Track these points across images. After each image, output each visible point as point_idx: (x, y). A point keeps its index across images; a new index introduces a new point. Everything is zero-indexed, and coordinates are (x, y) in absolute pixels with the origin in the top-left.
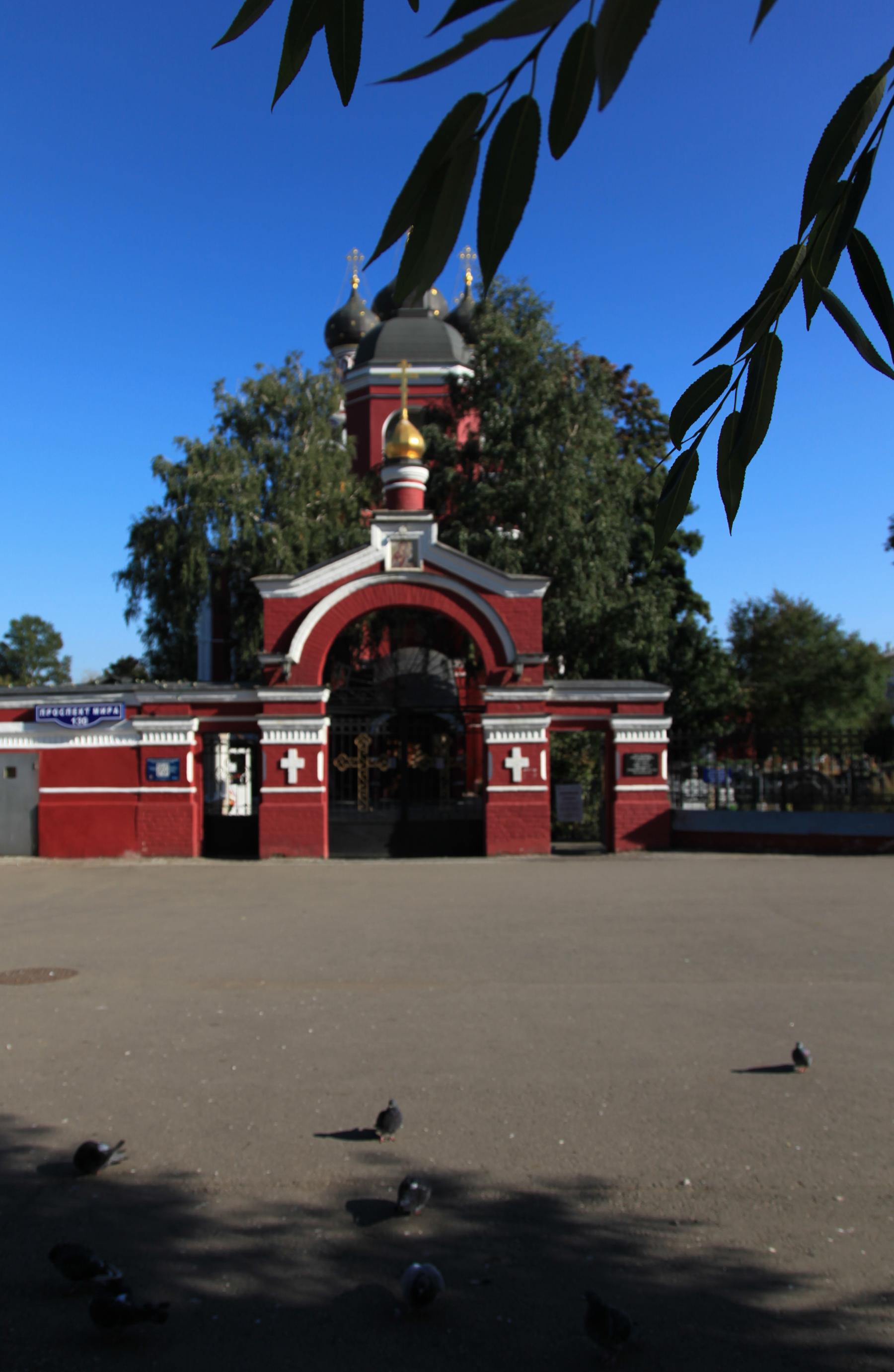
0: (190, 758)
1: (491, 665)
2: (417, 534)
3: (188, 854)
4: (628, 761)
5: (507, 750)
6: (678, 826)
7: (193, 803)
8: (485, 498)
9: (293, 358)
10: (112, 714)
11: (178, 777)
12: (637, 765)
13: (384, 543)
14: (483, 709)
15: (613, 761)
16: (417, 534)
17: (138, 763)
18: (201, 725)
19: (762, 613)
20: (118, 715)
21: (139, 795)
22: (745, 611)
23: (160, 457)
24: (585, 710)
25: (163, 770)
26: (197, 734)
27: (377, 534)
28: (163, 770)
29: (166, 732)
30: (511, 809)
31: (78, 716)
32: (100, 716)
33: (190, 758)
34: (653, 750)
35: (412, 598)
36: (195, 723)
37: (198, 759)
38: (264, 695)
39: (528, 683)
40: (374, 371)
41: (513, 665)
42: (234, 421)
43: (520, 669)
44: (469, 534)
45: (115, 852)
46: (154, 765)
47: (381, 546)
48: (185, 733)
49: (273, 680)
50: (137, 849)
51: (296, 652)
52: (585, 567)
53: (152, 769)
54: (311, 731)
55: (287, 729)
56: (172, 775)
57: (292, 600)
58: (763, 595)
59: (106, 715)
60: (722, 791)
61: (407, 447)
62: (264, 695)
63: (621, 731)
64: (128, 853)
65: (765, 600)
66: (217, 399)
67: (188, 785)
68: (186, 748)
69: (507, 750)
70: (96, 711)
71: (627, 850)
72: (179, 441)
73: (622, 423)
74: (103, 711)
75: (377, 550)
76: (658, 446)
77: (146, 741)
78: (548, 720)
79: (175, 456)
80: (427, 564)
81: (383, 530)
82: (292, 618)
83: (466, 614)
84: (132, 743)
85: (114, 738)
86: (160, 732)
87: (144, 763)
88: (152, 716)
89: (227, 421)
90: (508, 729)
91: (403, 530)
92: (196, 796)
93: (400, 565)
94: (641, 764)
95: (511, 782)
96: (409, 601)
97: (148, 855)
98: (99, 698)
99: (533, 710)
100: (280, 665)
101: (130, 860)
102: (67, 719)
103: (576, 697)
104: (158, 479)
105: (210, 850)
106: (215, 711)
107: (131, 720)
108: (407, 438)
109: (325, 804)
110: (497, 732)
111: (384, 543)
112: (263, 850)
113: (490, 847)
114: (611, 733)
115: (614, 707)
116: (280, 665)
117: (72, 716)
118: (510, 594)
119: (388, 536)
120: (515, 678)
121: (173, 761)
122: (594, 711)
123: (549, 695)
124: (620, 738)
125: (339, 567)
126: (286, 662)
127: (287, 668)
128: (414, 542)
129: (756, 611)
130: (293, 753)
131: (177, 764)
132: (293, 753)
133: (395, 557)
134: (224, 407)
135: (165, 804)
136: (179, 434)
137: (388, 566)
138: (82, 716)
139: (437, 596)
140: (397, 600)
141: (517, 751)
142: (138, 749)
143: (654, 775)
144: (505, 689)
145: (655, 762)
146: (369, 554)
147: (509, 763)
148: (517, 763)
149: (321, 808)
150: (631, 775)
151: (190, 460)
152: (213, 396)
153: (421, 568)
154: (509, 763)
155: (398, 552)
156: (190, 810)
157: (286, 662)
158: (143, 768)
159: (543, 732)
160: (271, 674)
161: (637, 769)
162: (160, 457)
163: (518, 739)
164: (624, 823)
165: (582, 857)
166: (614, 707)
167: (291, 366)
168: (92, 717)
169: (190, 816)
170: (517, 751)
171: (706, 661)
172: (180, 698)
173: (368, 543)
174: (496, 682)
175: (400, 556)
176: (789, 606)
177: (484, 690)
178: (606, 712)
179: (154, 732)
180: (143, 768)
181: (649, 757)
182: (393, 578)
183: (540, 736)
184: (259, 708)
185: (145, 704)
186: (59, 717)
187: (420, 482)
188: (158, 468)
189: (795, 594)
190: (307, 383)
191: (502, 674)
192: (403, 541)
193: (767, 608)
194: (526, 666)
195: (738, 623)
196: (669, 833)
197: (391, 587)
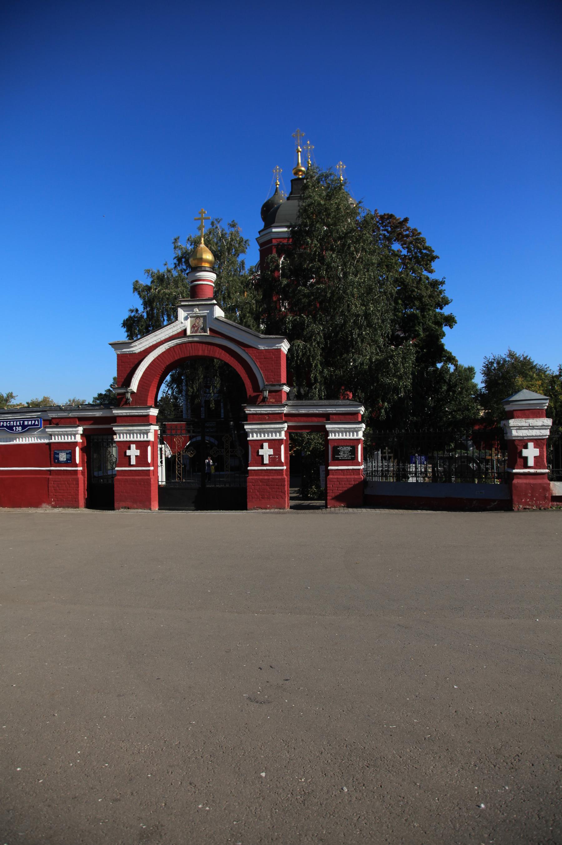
0: (77, 449)
1: (250, 392)
2: (205, 312)
3: (77, 507)
4: (336, 451)
5: (260, 444)
6: (368, 492)
7: (80, 476)
8: (305, 296)
9: (215, 222)
10: (34, 425)
11: (71, 461)
12: (341, 453)
13: (186, 318)
14: (246, 418)
15: (327, 452)
16: (205, 312)
17: (49, 453)
18: (84, 430)
19: (501, 364)
20: (38, 425)
21: (50, 471)
22: (492, 363)
23: (137, 282)
24: (310, 419)
25: (63, 457)
26: (82, 435)
27: (182, 314)
28: (63, 457)
29: (64, 435)
30: (262, 480)
31: (17, 426)
32: (28, 425)
33: (77, 449)
34: (353, 443)
35: (202, 351)
36: (80, 430)
37: (82, 450)
38: (116, 412)
39: (273, 403)
40: (274, 230)
41: (262, 391)
42: (183, 260)
43: (266, 394)
44: (293, 317)
45: (37, 505)
46: (58, 454)
47: (184, 321)
48: (75, 435)
49: (122, 403)
50: (49, 503)
51: (134, 386)
52: (360, 335)
53: (57, 456)
54: (144, 434)
55: (130, 433)
56: (67, 460)
57: (133, 355)
58: (502, 353)
59: (31, 425)
60: (423, 470)
61: (201, 260)
62: (116, 412)
63: (332, 432)
64: (44, 505)
65: (504, 356)
66: (175, 248)
67: (76, 466)
68: (75, 444)
69: (260, 444)
70: (26, 423)
71: (335, 507)
72: (148, 271)
73: (404, 252)
74: (30, 423)
75: (182, 323)
76: (426, 265)
77: (53, 440)
78: (286, 425)
79: (146, 281)
80: (211, 330)
81: (184, 311)
82: (133, 366)
83: (235, 360)
84: (46, 441)
85: (37, 439)
86: (61, 435)
87: (52, 452)
88: (57, 425)
89: (179, 260)
90: (260, 431)
91: (196, 310)
92: (83, 472)
93: (196, 332)
94: (344, 452)
95: (263, 464)
96: (200, 353)
97: (54, 507)
98: (28, 416)
99: (276, 419)
100: (124, 394)
101: (45, 510)
102: (11, 428)
103: (303, 411)
104: (136, 294)
105: (91, 504)
106: (92, 422)
107: (45, 428)
108: (202, 255)
109: (286, 477)
110: (254, 432)
111: (186, 318)
112: (116, 505)
113: (249, 505)
114: (327, 433)
115: (328, 417)
116: (124, 394)
117: (14, 426)
118: (262, 347)
119: (188, 314)
120: (264, 400)
121: (68, 452)
122: (315, 419)
123: (285, 410)
124: (331, 437)
125: (160, 334)
126: (128, 392)
127: (129, 396)
128: (204, 317)
129: (498, 363)
130: (133, 446)
131: (70, 453)
132: (133, 446)
133: (193, 327)
134: (179, 253)
135: (64, 477)
136: (148, 268)
137: (189, 333)
138: (19, 426)
139: (218, 349)
140: (193, 353)
141: (266, 445)
142: (49, 444)
143: (353, 460)
144: (259, 406)
145: (354, 452)
146: (177, 325)
147: (261, 452)
148: (266, 452)
149: (283, 480)
150: (338, 459)
151: (152, 282)
152: (173, 246)
153: (208, 333)
154: (261, 452)
155: (195, 324)
156: (77, 480)
157: (128, 392)
158: (52, 455)
159: (283, 433)
160: (122, 399)
161: (341, 455)
162: (137, 282)
163: (268, 438)
164: (333, 490)
165: (316, 511)
166: (328, 417)
167: (214, 227)
168: (24, 427)
169: (78, 484)
170: (266, 445)
171: (454, 392)
172: (70, 415)
173: (176, 318)
174: (253, 402)
175: (196, 326)
176: (517, 359)
177: (245, 407)
178: (324, 420)
179: (58, 435)
180: (52, 455)
181: (349, 448)
182: (191, 339)
183: (280, 436)
184: (114, 420)
185: (53, 418)
186: (7, 427)
187: (211, 281)
188: (136, 288)
189: (520, 352)
190: (223, 235)
191: (258, 396)
192: (197, 317)
193: (505, 361)
194: (270, 392)
195: (488, 371)
196: (361, 496)
197: (184, 345)
